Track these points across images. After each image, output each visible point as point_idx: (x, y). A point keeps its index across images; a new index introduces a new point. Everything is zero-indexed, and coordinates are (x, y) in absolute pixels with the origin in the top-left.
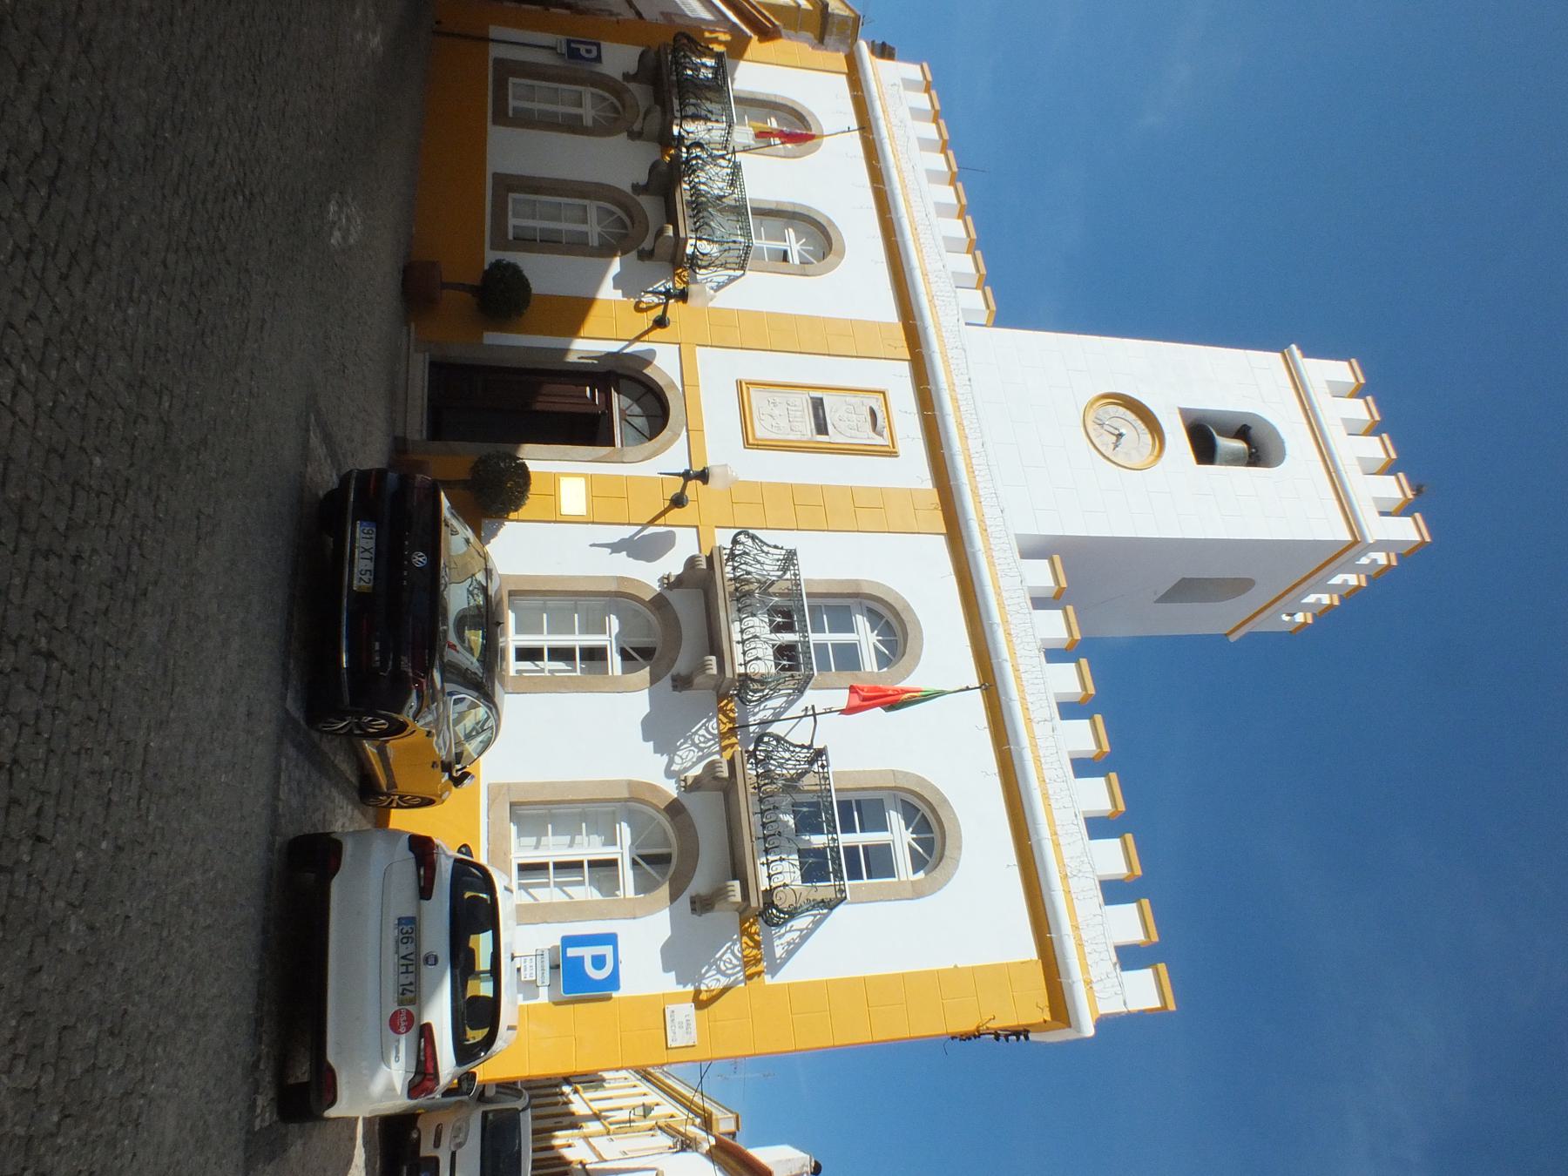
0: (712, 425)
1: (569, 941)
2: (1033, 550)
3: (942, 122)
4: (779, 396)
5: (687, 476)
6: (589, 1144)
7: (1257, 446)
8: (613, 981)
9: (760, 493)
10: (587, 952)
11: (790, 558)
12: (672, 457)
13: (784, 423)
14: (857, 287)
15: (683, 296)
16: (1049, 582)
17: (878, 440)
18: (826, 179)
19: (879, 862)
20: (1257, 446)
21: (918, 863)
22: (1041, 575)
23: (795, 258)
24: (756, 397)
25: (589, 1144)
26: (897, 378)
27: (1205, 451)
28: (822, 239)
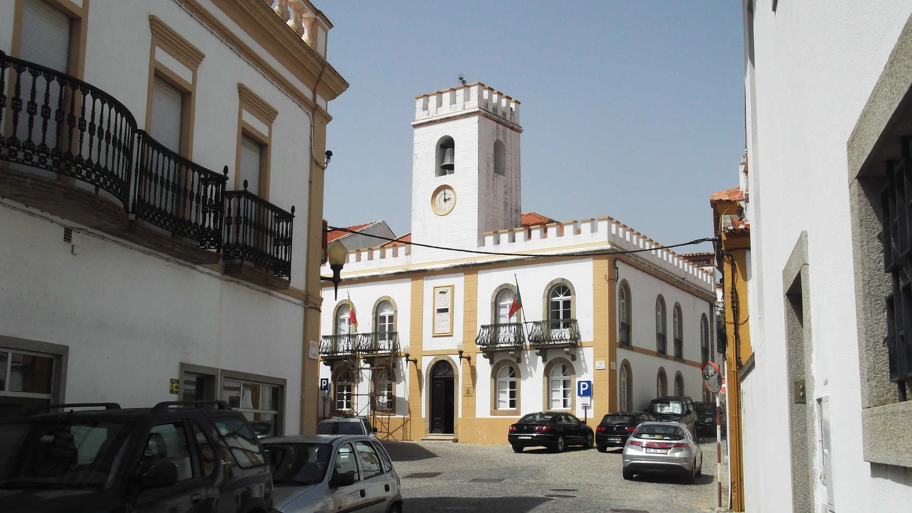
0: (448, 346)
1: (579, 394)
2: (482, 242)
3: (104, 408)
4: (437, 324)
5: (461, 357)
6: (351, 282)
7: (447, 145)
8: (589, 382)
9: (467, 332)
10: (582, 389)
11: (483, 327)
12: (456, 358)
13: (445, 323)
14: (400, 292)
15: (407, 356)
16: (507, 235)
17: (449, 292)
18: (363, 300)
19: (567, 304)
20: (447, 145)
21: (568, 294)
22: (489, 240)
23: (392, 313)
24: (438, 331)
25: (351, 282)
26: (429, 285)
27: (451, 168)
28: (383, 303)
